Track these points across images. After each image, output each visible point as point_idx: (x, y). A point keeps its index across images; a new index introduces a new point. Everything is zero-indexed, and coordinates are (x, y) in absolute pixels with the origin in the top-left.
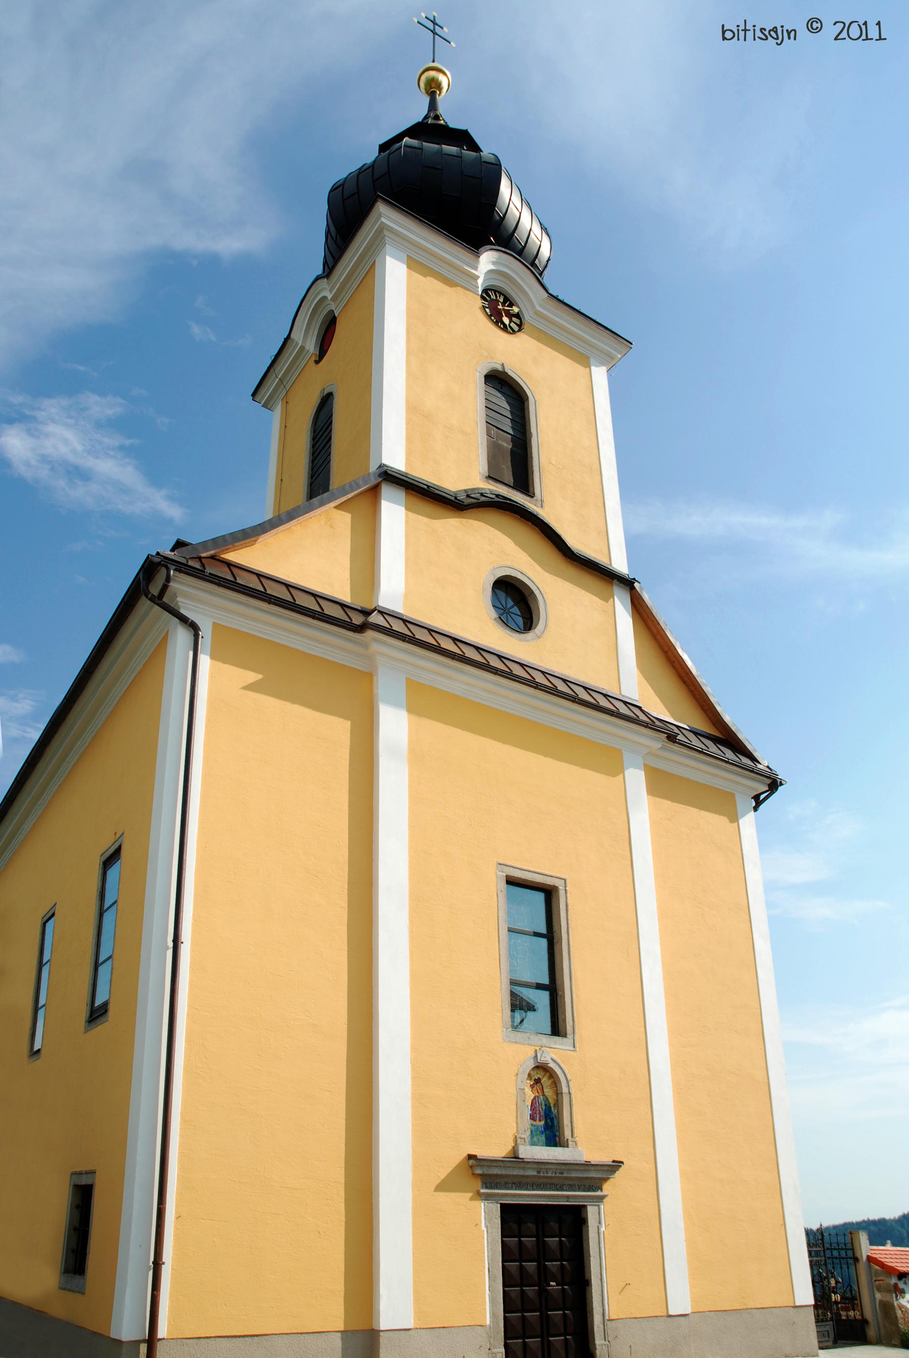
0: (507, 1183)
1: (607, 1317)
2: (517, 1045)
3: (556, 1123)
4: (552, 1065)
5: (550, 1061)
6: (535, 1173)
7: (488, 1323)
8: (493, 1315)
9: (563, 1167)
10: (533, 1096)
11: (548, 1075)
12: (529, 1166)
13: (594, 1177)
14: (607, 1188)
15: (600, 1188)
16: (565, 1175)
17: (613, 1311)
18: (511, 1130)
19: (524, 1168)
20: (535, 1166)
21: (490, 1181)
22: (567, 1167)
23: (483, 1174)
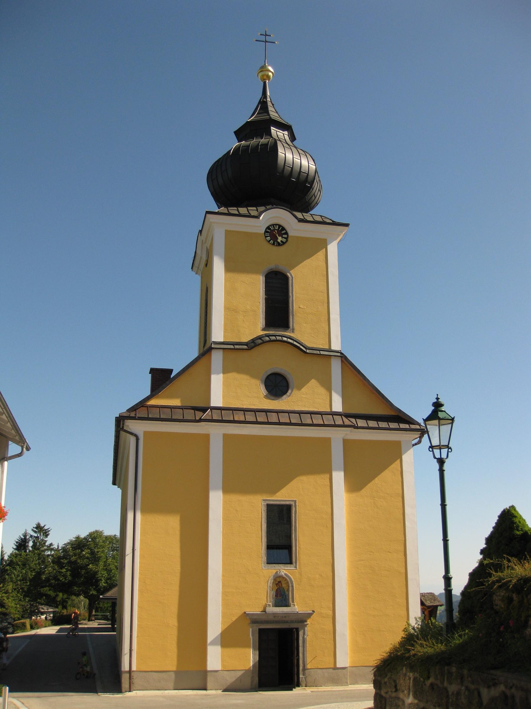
13: (302, 620)
23: (254, 620)
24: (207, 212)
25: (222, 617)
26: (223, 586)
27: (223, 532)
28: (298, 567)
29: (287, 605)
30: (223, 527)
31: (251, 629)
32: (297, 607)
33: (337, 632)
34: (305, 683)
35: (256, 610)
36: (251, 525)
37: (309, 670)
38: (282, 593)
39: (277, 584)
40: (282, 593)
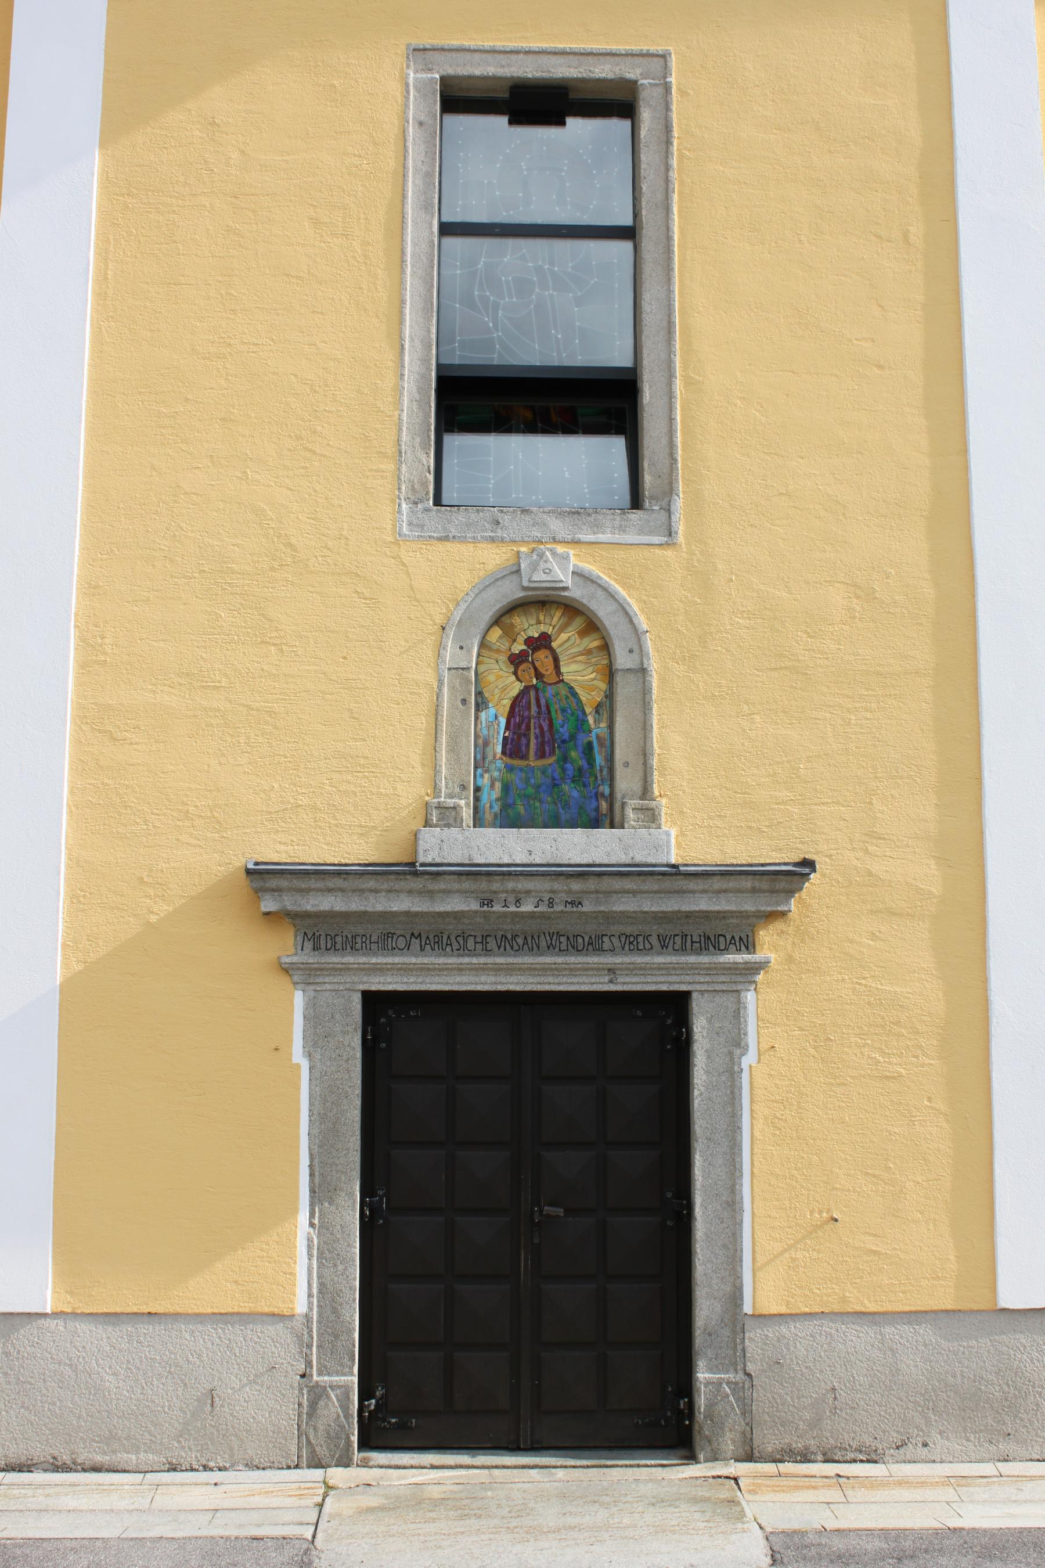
0: (390, 935)
1: (748, 1309)
2: (448, 545)
3: (599, 760)
4: (577, 592)
5: (568, 581)
6: (475, 906)
7: (300, 1307)
8: (326, 1294)
9: (576, 886)
10: (517, 688)
11: (578, 623)
12: (442, 885)
13: (735, 909)
14: (770, 944)
15: (747, 944)
16: (587, 907)
17: (763, 1290)
18: (409, 790)
19: (431, 894)
20: (467, 884)
21: (323, 933)
22: (591, 884)
23: (302, 907)
24: (438, 502)
25: (73, 898)
26: (84, 666)
27: (102, 278)
28: (681, 528)
29: (601, 816)
30: (103, 238)
31: (299, 999)
32: (689, 814)
33: (995, 1030)
34: (740, 1425)
35: (343, 836)
36: (316, 222)
37: (770, 1332)
38: (556, 742)
39: (516, 661)
40: (556, 742)
